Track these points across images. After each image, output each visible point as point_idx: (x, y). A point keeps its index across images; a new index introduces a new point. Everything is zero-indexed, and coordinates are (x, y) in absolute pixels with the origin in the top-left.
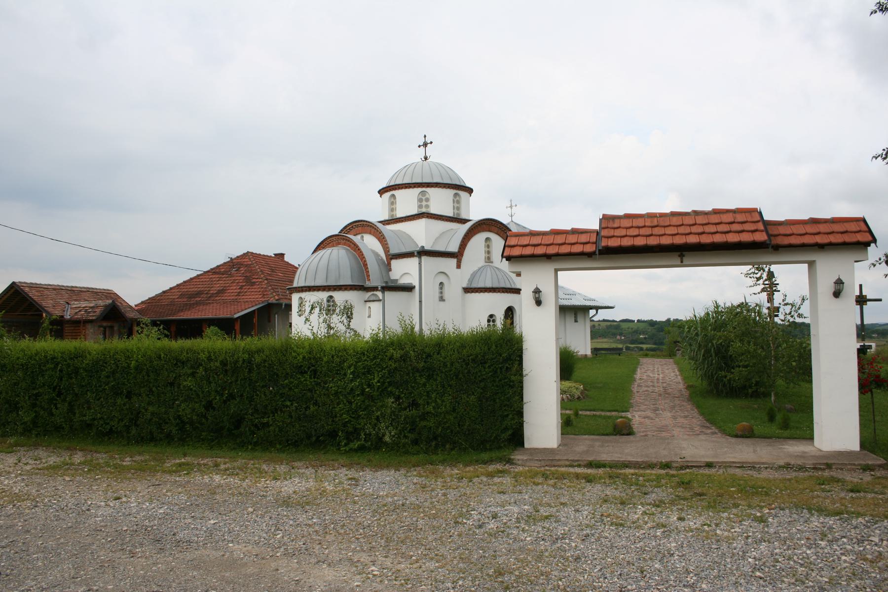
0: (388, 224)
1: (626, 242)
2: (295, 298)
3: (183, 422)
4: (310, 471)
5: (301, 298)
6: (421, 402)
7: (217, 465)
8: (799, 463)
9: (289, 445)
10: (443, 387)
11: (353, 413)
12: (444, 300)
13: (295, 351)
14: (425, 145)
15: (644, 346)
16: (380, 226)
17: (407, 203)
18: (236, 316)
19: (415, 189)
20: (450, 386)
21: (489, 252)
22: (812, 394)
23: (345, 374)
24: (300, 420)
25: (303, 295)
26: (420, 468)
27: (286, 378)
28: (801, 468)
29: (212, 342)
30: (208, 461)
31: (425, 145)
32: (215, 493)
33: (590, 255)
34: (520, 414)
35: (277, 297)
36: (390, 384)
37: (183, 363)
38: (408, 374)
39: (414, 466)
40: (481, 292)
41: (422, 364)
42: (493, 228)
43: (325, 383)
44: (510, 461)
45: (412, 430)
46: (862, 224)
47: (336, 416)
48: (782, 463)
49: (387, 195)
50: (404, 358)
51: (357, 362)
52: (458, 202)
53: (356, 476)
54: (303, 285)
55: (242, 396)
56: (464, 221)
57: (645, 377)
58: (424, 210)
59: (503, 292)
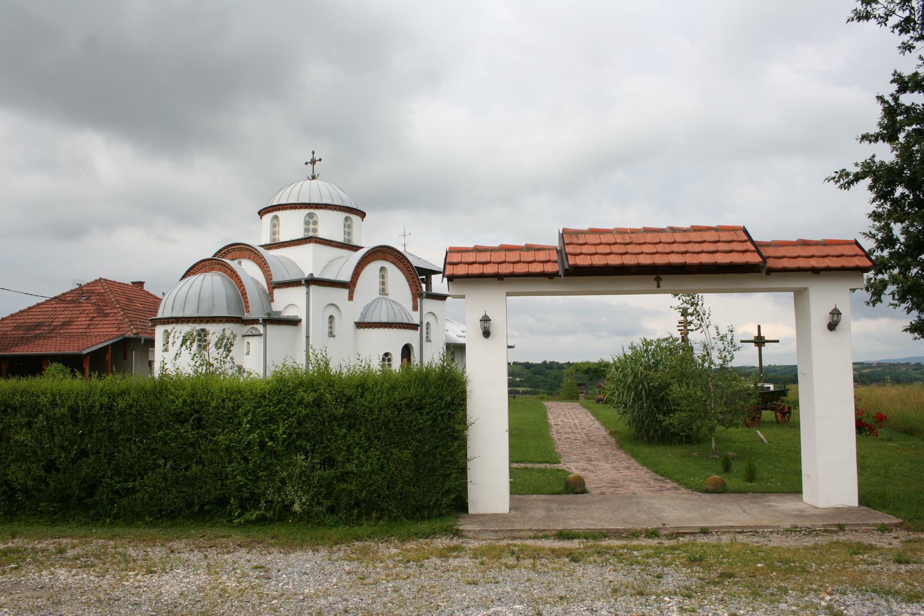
0: (270, 249)
1: (598, 261)
2: (159, 331)
3: (11, 489)
4: (196, 557)
5: (166, 331)
6: (339, 458)
7: (61, 551)
8: (808, 524)
9: (162, 516)
10: (368, 439)
11: (250, 475)
12: (334, 336)
13: (172, 394)
14: (313, 162)
15: (520, 389)
16: (261, 250)
17: (292, 225)
18: (85, 352)
19: (302, 210)
20: (377, 438)
21: (383, 283)
22: (799, 444)
23: (240, 424)
24: (178, 483)
25: (169, 327)
26: (343, 547)
27: (160, 429)
28: (811, 532)
29: (55, 382)
30: (48, 544)
31: (313, 162)
32: (59, 603)
33: (551, 276)
34: (464, 471)
35: (135, 331)
36: (299, 435)
37: (15, 409)
38: (323, 423)
39: (336, 543)
40: (376, 327)
41: (342, 410)
42: (389, 256)
43: (213, 435)
44: (458, 533)
45: (328, 495)
46: (856, 247)
47: (227, 478)
48: (787, 525)
49: (268, 217)
50: (318, 403)
51: (255, 408)
52: (349, 227)
53: (262, 561)
54: (169, 315)
55: (98, 452)
56: (356, 248)
57: (560, 423)
58: (311, 234)
59: (400, 328)
